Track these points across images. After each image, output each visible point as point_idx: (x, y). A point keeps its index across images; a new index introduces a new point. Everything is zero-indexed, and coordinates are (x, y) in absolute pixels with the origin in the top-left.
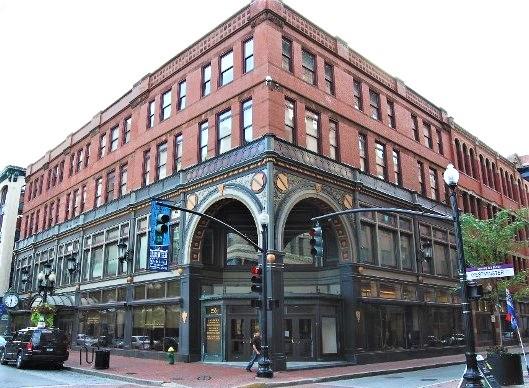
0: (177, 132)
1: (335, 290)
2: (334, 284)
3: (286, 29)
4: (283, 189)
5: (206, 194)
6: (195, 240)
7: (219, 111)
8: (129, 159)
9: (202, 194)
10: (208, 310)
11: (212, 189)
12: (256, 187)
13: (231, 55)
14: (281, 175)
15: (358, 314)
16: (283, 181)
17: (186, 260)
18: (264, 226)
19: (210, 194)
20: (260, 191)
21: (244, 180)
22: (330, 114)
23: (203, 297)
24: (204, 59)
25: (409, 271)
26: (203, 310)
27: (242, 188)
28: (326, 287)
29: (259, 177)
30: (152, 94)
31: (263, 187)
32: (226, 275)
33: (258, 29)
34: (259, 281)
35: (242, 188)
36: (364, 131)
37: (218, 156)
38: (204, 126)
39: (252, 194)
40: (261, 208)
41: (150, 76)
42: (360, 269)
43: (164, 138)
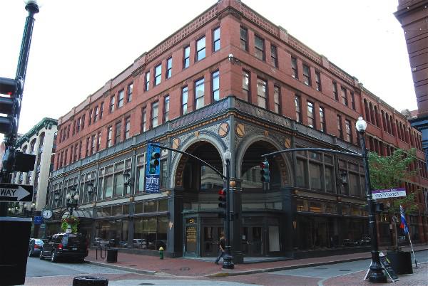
0: (165, 94)
1: (279, 206)
2: (277, 202)
3: (243, 20)
4: (242, 134)
5: (186, 138)
6: (178, 171)
7: (195, 79)
8: (131, 113)
9: (183, 138)
10: (188, 221)
11: (190, 134)
12: (222, 133)
13: (204, 39)
14: (240, 125)
15: (295, 223)
16: (241, 130)
17: (172, 185)
18: (228, 161)
19: (189, 138)
20: (225, 136)
21: (213, 128)
22: (275, 81)
23: (184, 211)
24: (185, 42)
25: (331, 193)
26: (184, 221)
27: (212, 134)
28: (271, 204)
29: (224, 126)
30: (148, 67)
31: (227, 133)
32: (201, 196)
33: (223, 21)
34: (224, 200)
35: (212, 134)
36: (299, 94)
37: (195, 111)
38: (184, 90)
39: (219, 138)
40: (225, 148)
41: (146, 54)
42: (296, 191)
43: (156, 98)
